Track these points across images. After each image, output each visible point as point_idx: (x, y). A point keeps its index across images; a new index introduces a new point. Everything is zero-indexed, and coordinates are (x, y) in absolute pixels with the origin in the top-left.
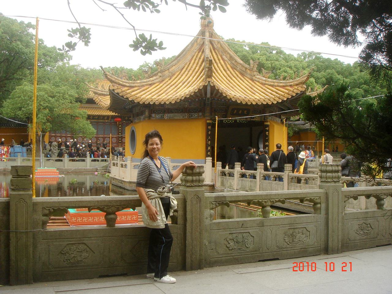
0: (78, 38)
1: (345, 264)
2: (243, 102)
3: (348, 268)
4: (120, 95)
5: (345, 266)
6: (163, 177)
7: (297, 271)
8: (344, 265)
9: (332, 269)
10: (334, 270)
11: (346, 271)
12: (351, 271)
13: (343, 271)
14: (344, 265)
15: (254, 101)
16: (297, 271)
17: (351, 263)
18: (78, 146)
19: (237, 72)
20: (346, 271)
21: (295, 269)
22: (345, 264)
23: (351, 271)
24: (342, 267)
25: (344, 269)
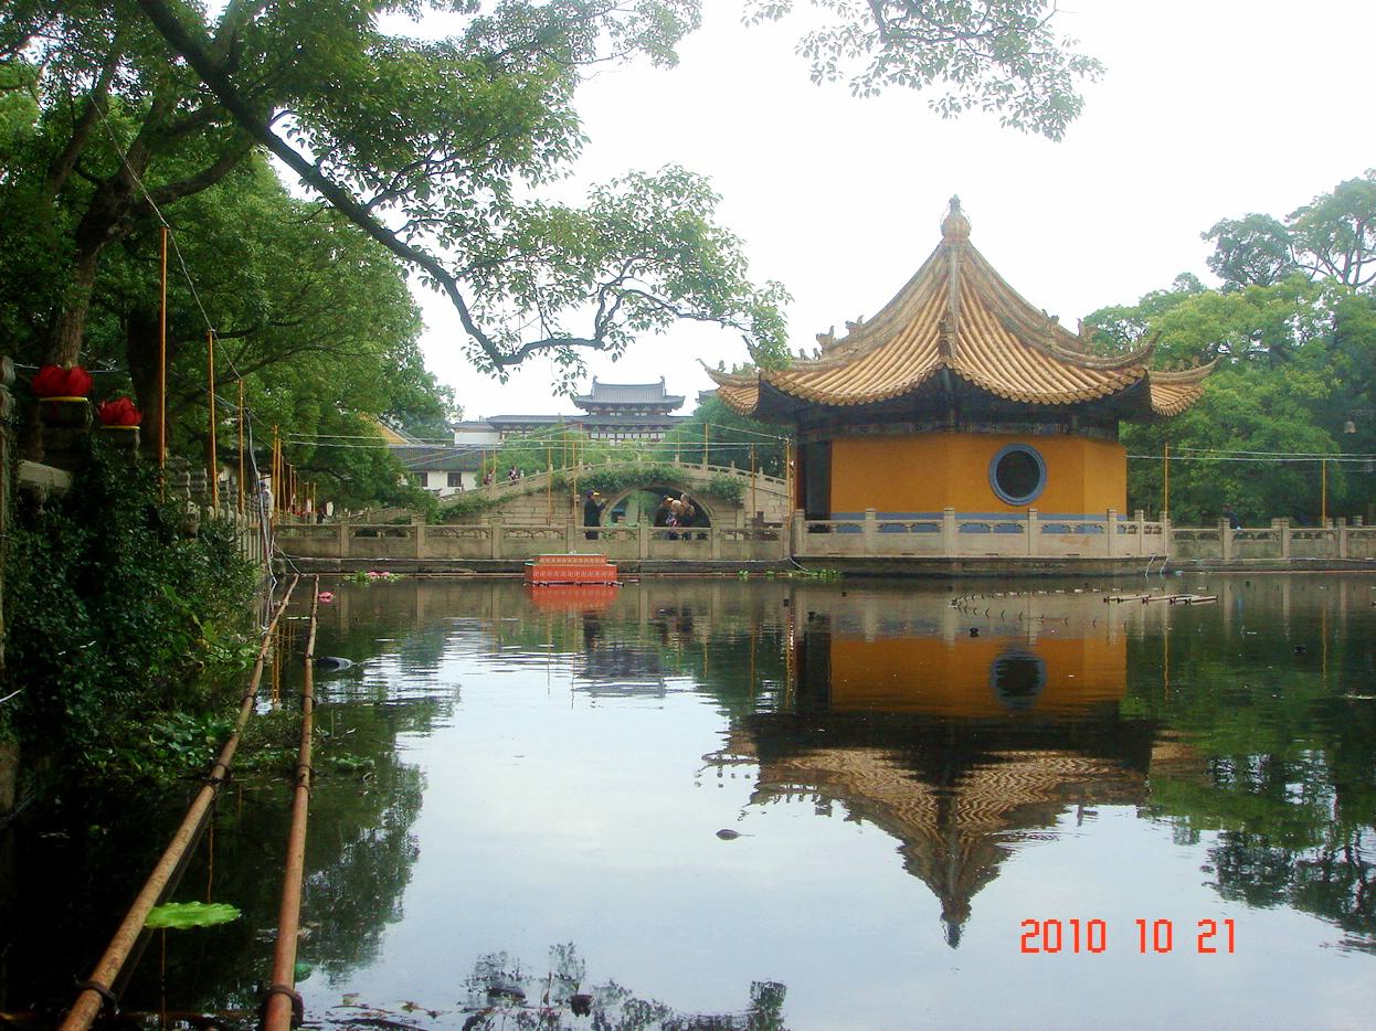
0: (1105, 536)
1: (1210, 926)
2: (1012, 398)
3: (1219, 940)
4: (773, 384)
5: (1208, 935)
6: (544, 521)
7: (1036, 950)
8: (1207, 928)
9: (1097, 944)
10: (1103, 948)
11: (1213, 950)
12: (1231, 950)
13: (1201, 950)
14: (1207, 928)
15: (1036, 397)
16: (1036, 950)
17: (1230, 922)
18: (1289, 787)
19: (1054, 363)
20: (1213, 950)
21: (1030, 943)
22: (1210, 926)
23: (1231, 950)
24: (1201, 938)
25: (1207, 943)
